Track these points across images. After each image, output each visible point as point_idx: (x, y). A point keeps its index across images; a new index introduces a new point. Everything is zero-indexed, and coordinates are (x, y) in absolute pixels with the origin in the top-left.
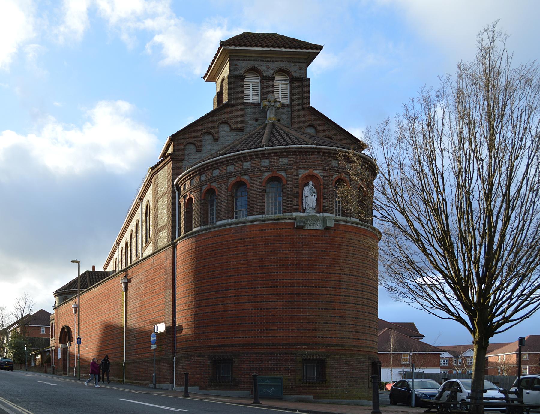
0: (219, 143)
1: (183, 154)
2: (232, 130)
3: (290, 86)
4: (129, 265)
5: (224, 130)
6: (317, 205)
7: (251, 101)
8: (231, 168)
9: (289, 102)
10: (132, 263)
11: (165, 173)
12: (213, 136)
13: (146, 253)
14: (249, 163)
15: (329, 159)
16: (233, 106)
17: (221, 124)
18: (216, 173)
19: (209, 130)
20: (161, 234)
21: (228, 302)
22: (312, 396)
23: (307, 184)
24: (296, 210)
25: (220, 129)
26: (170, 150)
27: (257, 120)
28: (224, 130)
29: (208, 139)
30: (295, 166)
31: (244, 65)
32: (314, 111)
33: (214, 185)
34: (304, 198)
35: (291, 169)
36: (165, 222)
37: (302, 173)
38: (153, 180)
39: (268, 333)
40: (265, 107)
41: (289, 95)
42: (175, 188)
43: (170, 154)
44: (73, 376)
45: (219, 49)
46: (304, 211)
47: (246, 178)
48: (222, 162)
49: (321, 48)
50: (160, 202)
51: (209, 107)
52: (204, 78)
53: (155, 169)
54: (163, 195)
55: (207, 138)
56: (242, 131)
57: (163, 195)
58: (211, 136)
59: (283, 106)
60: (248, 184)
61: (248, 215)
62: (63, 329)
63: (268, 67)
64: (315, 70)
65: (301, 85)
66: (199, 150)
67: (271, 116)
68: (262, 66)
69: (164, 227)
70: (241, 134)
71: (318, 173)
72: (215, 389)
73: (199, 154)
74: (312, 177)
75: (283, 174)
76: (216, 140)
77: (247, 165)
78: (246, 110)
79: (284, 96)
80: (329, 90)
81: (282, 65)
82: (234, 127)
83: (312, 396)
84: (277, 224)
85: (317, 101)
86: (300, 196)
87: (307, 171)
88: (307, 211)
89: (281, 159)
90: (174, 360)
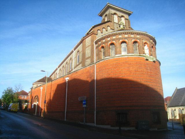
2: (111, 29)
37: (144, 41)
38: (83, 42)
71: (147, 42)
76: (107, 31)
82: (112, 28)
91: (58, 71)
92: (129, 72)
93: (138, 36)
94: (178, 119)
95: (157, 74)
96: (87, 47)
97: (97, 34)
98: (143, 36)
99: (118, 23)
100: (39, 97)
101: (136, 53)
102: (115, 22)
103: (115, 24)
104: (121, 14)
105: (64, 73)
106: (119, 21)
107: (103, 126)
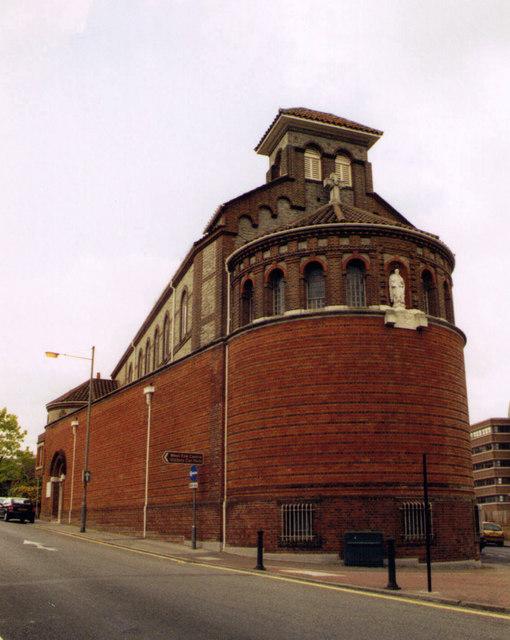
0: (278, 220)
1: (237, 227)
2: (293, 207)
3: (352, 169)
4: (151, 371)
5: (283, 207)
6: (406, 298)
7: (312, 178)
8: (303, 246)
9: (350, 185)
10: (156, 369)
11: (210, 253)
12: (271, 212)
13: (181, 354)
14: (325, 241)
15: (414, 245)
16: (293, 180)
17: (280, 198)
18: (284, 250)
19: (266, 203)
20: (205, 327)
21: (302, 422)
22: (416, 560)
23: (393, 272)
24: (384, 303)
25: (280, 204)
26: (221, 222)
27: (319, 200)
28: (283, 207)
29: (265, 215)
30: (379, 249)
31: (302, 140)
32: (376, 197)
33: (282, 265)
34: (390, 289)
35: (375, 251)
36: (212, 311)
37: (388, 258)
38: (196, 259)
39: (357, 468)
40: (328, 186)
41: (350, 177)
42: (227, 268)
43: (220, 227)
44: (67, 524)
45: (278, 117)
46: (392, 304)
47: (322, 259)
48: (292, 237)
49: (382, 133)
50: (205, 286)
51: (262, 181)
52: (256, 149)
53: (199, 247)
54: (210, 277)
55: (263, 212)
56: (303, 209)
57: (210, 277)
58: (268, 212)
59: (347, 188)
60: (325, 266)
61: (326, 305)
62: (57, 454)
63: (329, 145)
64: (373, 155)
65: (362, 167)
66: (255, 226)
67: (335, 195)
68: (323, 142)
69: (210, 318)
70: (302, 213)
71: (404, 260)
72: (288, 551)
73: (255, 230)
74: (400, 265)
75: (365, 257)
76: (274, 216)
77: (323, 243)
78: (307, 188)
79: (346, 176)
80: (394, 177)
81: (343, 145)
82: (294, 203)
83: (416, 560)
84: (364, 318)
85: (381, 186)
86: (386, 286)
87: (393, 257)
88: (396, 305)
89: (363, 239)
90: (224, 506)
91: (133, 359)
92: (323, 369)
93: (366, 242)
94: (24, 457)
95: (435, 374)
96: (206, 280)
97: (344, 192)
98: (384, 239)
99: (322, 183)
100: (68, 455)
101: (356, 302)
102: (311, 176)
103: (310, 187)
104: (330, 147)
105: (151, 366)
106: (325, 174)
107: (235, 548)
